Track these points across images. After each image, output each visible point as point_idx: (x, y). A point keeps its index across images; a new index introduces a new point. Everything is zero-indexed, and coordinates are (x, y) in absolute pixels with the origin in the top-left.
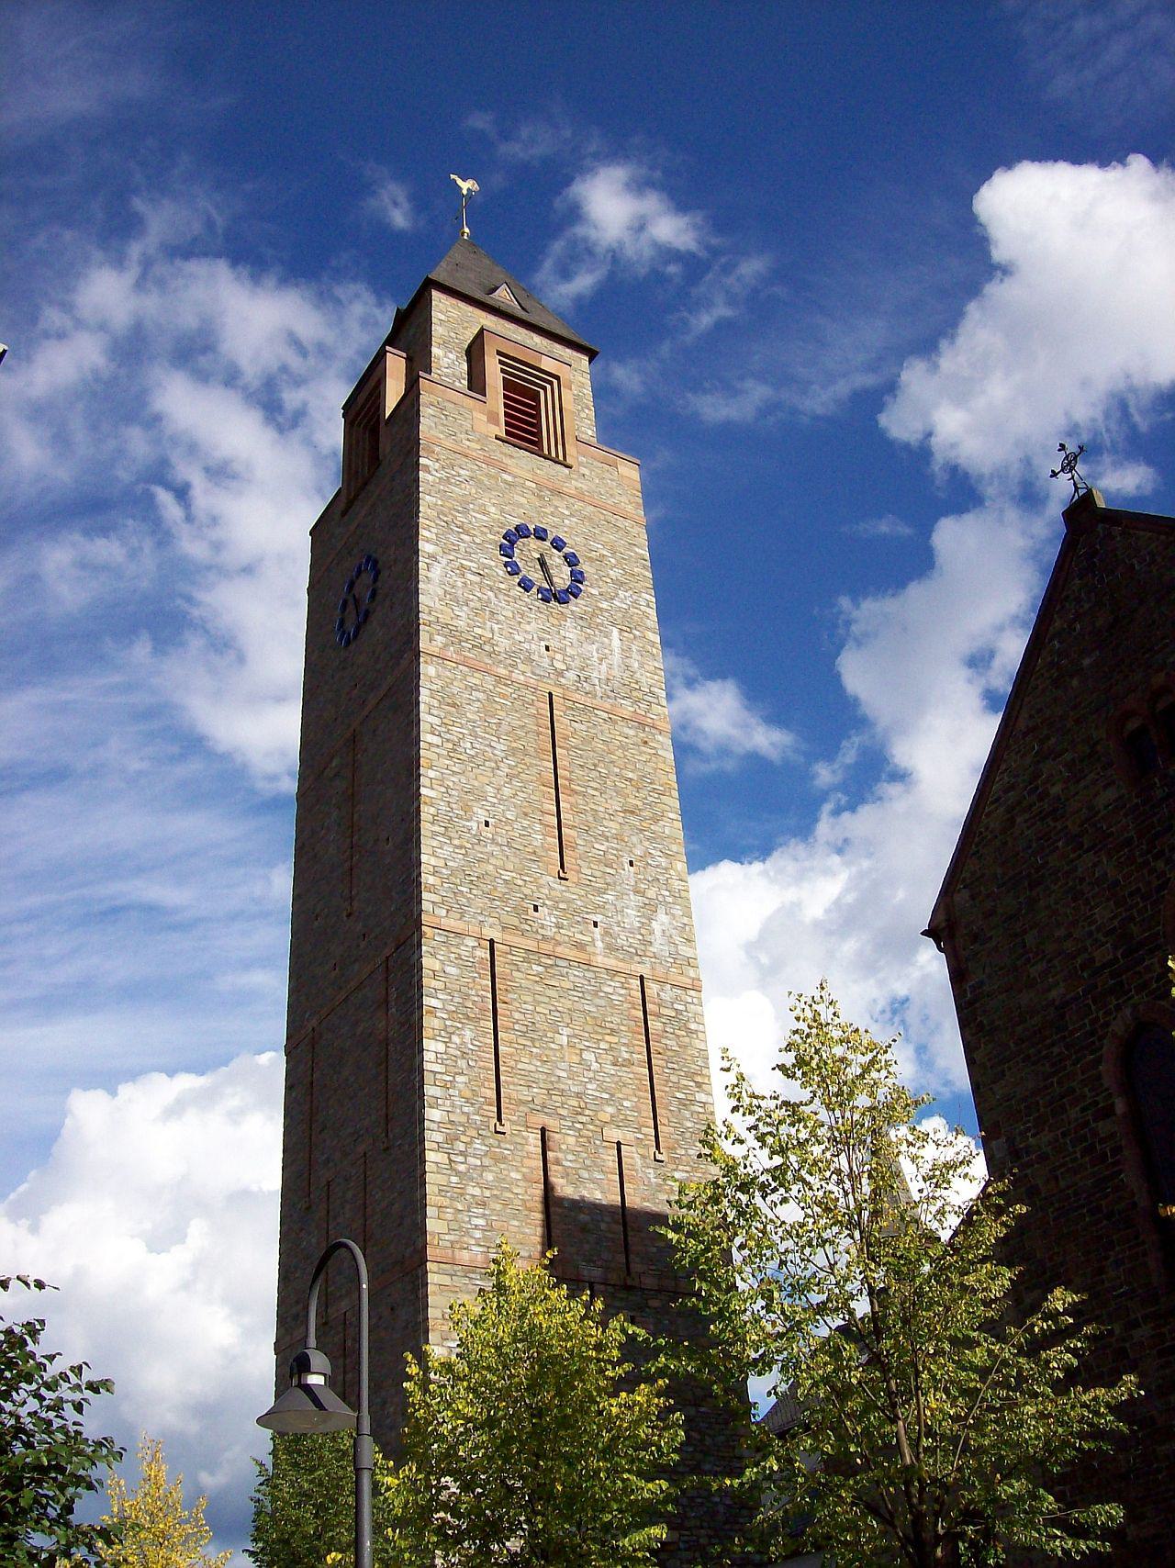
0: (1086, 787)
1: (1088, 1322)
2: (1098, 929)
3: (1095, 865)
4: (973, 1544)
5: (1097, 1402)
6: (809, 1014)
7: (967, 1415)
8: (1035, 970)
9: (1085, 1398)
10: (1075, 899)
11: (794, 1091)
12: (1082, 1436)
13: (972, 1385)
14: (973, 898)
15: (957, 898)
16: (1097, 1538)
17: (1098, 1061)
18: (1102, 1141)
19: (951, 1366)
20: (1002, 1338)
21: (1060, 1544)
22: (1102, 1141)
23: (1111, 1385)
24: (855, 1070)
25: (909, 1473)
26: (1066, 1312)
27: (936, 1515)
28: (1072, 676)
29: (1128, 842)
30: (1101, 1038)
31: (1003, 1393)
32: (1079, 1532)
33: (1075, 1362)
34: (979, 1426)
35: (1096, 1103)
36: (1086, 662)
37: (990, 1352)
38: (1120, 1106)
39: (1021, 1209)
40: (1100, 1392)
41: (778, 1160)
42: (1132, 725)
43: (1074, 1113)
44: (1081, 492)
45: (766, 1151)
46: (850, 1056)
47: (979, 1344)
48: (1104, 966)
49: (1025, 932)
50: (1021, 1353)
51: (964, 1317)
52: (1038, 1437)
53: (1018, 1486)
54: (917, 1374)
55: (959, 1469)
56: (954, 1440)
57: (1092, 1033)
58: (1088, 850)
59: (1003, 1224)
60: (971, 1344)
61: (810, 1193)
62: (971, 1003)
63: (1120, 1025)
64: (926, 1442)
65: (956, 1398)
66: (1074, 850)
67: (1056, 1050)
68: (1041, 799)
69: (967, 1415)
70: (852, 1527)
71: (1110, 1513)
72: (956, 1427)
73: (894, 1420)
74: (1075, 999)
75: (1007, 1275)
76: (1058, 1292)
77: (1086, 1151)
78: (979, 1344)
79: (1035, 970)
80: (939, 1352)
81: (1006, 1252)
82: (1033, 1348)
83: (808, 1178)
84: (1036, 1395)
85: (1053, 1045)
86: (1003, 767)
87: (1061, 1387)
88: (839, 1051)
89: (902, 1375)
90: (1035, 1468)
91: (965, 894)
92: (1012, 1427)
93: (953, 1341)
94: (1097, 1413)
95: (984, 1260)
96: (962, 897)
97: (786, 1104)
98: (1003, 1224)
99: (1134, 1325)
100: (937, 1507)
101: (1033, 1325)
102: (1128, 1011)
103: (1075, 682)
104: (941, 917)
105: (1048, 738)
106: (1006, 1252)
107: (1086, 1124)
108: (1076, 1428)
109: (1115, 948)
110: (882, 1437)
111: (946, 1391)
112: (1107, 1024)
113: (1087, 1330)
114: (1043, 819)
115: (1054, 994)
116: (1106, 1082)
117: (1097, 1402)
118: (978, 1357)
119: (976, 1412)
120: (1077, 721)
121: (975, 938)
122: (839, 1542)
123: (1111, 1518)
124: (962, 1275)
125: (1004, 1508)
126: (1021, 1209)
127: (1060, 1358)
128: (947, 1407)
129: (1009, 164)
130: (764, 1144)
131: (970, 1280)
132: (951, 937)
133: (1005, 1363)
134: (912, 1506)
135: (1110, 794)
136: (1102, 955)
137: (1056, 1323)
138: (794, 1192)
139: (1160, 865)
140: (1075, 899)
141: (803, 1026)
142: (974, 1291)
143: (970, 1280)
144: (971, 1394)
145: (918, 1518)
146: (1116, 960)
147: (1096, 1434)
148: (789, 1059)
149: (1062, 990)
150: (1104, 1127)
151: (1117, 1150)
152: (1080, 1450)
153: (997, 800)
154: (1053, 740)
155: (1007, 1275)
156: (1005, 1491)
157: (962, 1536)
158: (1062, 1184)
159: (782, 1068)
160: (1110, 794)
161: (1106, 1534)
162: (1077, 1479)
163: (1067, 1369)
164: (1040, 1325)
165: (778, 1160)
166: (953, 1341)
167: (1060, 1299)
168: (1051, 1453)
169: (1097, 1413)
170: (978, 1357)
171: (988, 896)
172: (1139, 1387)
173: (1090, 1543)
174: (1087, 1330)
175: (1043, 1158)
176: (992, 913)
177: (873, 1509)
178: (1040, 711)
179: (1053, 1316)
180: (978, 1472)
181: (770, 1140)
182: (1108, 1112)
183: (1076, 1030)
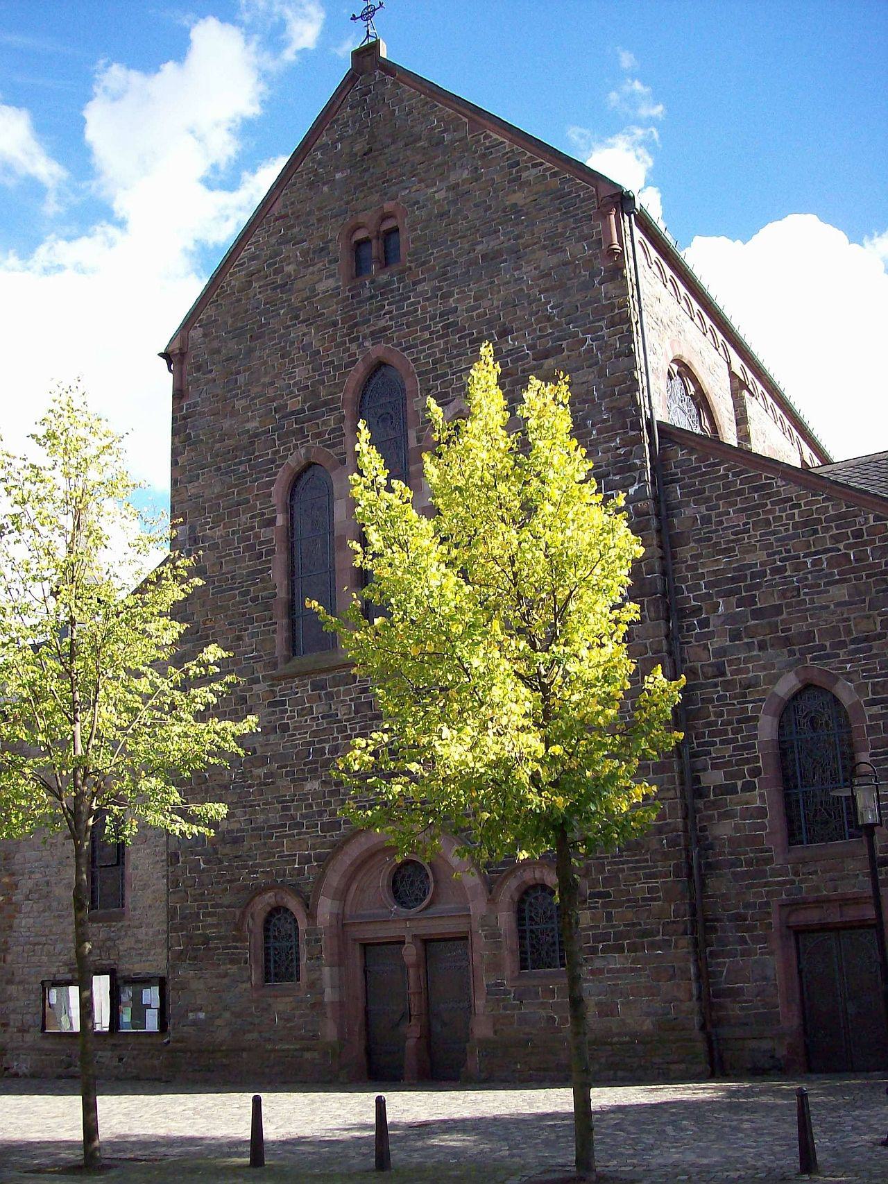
0: (313, 273)
1: (230, 673)
2: (295, 384)
3: (304, 335)
4: (116, 819)
5: (229, 732)
6: (64, 399)
7: (129, 726)
8: (240, 404)
9: (218, 728)
10: (283, 357)
11: (40, 456)
12: (211, 754)
13: (136, 705)
14: (205, 335)
15: (192, 333)
16: (205, 826)
17: (271, 483)
18: (261, 543)
19: (122, 690)
20: (163, 674)
21: (178, 826)
22: (261, 543)
23: (238, 719)
24: (90, 452)
25: (81, 764)
26: (215, 664)
27: (93, 794)
28: (324, 184)
29: (335, 324)
30: (279, 466)
31: (158, 714)
32: (192, 819)
33: (215, 701)
34: (135, 735)
35: (263, 514)
36: (338, 176)
37: (152, 684)
38: (280, 520)
39: (198, 581)
40: (228, 724)
41: (17, 509)
42: (360, 235)
43: (245, 518)
44: (371, 40)
45: (11, 500)
46: (90, 437)
47: (145, 675)
48: (293, 413)
49: (238, 373)
50: (176, 688)
51: (140, 653)
52: (180, 750)
53: (155, 783)
54: (97, 691)
55: (116, 765)
56: (115, 743)
57: (273, 461)
58: (304, 321)
59: (183, 590)
60: (139, 675)
61: (39, 539)
62: (185, 418)
63: (295, 460)
64: (94, 742)
65: (121, 713)
66: (291, 319)
67: (242, 468)
68: (276, 272)
69: (129, 726)
70: (28, 796)
71: (218, 810)
72: (118, 733)
73: (73, 723)
74: (267, 432)
75: (179, 627)
76: (212, 648)
77: (247, 549)
78: (145, 675)
79: (240, 404)
80: (117, 678)
81: (178, 612)
82: (184, 687)
83: (38, 526)
84: (181, 720)
85: (241, 463)
86: (253, 240)
87: (200, 717)
88: (82, 433)
89: (85, 689)
90: (172, 775)
91: (200, 331)
92: (164, 740)
93: (128, 671)
94: (224, 739)
95: (161, 614)
96: (196, 333)
97: (34, 467)
98: (183, 590)
99: (255, 681)
100: (94, 789)
101: (188, 669)
102: (303, 451)
103: (325, 189)
104: (177, 345)
105: (293, 226)
106: (178, 612)
107: (253, 528)
108: (208, 747)
109: (305, 402)
110: (62, 733)
111: (115, 705)
112: (285, 457)
113: (229, 678)
114: (274, 289)
115: (249, 426)
116: (274, 500)
117: (229, 732)
118: (143, 685)
119: (135, 725)
120: (319, 220)
121: (199, 368)
122: (14, 805)
123: (218, 813)
124: (145, 621)
125: (144, 798)
126: (198, 581)
127: (204, 696)
128: (114, 719)
129: (825, 218)
130: (9, 494)
131: (151, 628)
132: (181, 362)
133: (163, 693)
134: (76, 786)
135: (331, 283)
136: (294, 404)
137: (206, 670)
138: (26, 537)
139: (353, 347)
140: (283, 357)
141: (56, 407)
142: (150, 636)
143: (151, 628)
144: (134, 711)
145: (80, 796)
146: (303, 411)
147: (221, 753)
148: (41, 431)
149: (257, 424)
150: (264, 533)
151: (270, 552)
152: (207, 763)
153: (241, 265)
154: (296, 230)
155: (179, 627)
156: (144, 785)
157: (110, 812)
158: (224, 569)
159: (33, 436)
160: (331, 283)
161: (213, 824)
162: (197, 783)
163: (207, 705)
164: (194, 669)
165: (17, 509)
166: (128, 671)
167: (213, 653)
168: (186, 763)
169: (224, 739)
170: (143, 685)
171: (217, 337)
172: (257, 725)
173: (200, 828)
174: (229, 678)
175: (214, 546)
176: (218, 351)
177: (47, 786)
178: (293, 203)
179: (205, 665)
180: (131, 770)
181: (14, 492)
182: (272, 522)
183: (260, 456)
